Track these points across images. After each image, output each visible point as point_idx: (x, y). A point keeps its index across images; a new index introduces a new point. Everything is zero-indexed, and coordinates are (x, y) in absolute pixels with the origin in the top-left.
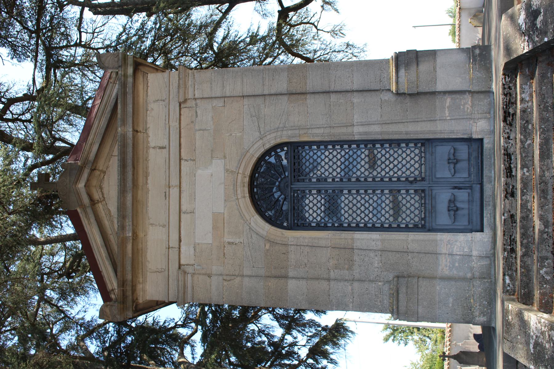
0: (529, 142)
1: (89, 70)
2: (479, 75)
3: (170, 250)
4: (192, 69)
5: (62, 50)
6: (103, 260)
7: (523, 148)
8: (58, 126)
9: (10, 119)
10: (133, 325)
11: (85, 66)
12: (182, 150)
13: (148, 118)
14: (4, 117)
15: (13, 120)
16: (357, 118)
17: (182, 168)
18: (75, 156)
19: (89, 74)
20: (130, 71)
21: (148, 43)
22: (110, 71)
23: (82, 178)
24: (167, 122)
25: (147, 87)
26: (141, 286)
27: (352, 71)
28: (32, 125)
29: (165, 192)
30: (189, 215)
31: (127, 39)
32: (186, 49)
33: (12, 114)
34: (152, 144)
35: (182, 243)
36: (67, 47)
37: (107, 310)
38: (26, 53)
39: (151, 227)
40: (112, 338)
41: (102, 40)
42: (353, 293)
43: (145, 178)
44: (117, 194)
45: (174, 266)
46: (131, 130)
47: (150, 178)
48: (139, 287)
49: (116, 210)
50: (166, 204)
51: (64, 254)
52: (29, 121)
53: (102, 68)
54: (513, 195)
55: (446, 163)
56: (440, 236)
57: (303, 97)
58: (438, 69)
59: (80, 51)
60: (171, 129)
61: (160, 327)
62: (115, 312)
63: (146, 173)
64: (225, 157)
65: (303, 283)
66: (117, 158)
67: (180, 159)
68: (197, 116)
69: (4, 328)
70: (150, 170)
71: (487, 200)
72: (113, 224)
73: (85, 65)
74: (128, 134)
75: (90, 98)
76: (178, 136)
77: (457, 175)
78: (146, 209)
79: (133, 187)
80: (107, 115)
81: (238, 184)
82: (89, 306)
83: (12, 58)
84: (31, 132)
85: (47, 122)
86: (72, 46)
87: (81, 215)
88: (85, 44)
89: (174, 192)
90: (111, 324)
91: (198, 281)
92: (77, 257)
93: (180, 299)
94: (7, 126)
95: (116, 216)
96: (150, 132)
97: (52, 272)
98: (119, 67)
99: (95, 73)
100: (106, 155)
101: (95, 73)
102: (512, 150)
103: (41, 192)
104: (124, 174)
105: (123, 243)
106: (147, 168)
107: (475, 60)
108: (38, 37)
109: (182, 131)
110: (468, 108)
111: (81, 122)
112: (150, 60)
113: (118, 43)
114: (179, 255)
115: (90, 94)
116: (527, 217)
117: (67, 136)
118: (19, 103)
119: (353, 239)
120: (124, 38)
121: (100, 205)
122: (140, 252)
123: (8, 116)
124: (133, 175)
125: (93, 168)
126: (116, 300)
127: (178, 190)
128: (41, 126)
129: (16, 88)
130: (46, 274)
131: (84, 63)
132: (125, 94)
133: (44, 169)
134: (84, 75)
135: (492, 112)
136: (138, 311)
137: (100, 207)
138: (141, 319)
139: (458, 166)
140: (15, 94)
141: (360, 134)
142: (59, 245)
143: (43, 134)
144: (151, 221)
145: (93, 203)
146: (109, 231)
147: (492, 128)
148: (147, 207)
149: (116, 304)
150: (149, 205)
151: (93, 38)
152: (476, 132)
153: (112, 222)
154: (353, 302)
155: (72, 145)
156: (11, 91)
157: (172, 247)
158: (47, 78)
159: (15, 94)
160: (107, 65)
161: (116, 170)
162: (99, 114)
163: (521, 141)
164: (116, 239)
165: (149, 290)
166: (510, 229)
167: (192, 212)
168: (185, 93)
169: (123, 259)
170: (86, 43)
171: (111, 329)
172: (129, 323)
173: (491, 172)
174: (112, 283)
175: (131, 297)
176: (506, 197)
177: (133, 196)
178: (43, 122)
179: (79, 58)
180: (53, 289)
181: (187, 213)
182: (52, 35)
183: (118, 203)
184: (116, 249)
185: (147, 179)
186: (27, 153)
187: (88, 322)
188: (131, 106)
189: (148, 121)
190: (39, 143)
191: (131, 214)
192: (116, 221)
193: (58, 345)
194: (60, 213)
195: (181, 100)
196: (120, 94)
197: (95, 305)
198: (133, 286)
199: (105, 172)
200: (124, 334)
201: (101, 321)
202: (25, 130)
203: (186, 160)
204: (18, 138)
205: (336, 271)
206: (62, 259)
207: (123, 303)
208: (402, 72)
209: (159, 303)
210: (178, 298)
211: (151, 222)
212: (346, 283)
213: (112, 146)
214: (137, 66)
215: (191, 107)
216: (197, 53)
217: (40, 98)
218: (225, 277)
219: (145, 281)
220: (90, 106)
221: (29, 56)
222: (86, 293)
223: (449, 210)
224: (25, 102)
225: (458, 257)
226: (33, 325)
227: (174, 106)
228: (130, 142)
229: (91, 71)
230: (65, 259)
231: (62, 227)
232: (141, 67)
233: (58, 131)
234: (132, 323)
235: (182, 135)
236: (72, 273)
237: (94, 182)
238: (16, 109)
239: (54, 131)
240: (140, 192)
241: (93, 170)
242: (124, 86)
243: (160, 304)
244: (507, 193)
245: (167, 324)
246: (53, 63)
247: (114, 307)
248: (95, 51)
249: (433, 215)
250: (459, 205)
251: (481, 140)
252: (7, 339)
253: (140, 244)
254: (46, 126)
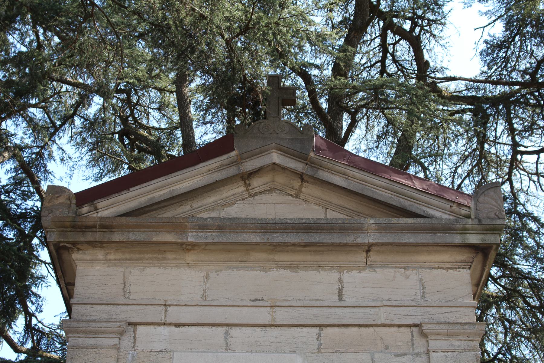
1: (473, 167)
3: (162, 308)
4: (482, 345)
5: (506, 121)
6: (148, 192)
8: (376, 117)
9: (386, 41)
10: (35, 241)
11: (480, 160)
12: (336, 329)
13: (392, 270)
14: (389, 32)
15: (384, 46)
17: (305, 329)
18: (324, 147)
19: (466, 167)
20: (474, 239)
21: (524, 266)
22: (472, 204)
23: (287, 159)
24: (385, 303)
25: (447, 269)
26: (101, 257)
28: (377, 75)
29: (262, 300)
30: (222, 341)
31: (530, 231)
32: (518, 334)
33: (394, 44)
34: (347, 277)
35: (173, 328)
36: (512, 131)
37: (62, 200)
38: (496, 64)
40: (13, 206)
41: (525, 189)
43: (288, 264)
44: (261, 217)
46: (371, 241)
47: (287, 273)
48: (100, 254)
49: (233, 215)
50: (242, 300)
51: (163, 126)
52: (383, 71)
53: (476, 191)
59: (505, 151)
60: (374, 310)
61: (28, 288)
62: (58, 212)
63: (297, 267)
66: (323, 217)
67: (320, 326)
68: (397, 355)
69: (41, 31)
70: (302, 274)
72: (210, 210)
73: (481, 160)
74: (363, 235)
75: (425, 169)
76: (361, 322)
78: (233, 267)
79: (271, 244)
80: (396, 200)
82: (71, 169)
83: (486, 42)
84: (365, 74)
85: (382, 100)
86: (513, 139)
87: (225, 157)
88: (517, 160)
89: (263, 315)
90: (39, 204)
91: (105, 357)
92: (156, 148)
93: (75, 324)
94: (374, 36)
95: (222, 215)
96: (367, 274)
97: (132, 106)
98: (480, 221)
99: (468, 176)
100: (327, 198)
101: (468, 176)
103: (263, 93)
104: (294, 228)
105: (176, 226)
106: (306, 268)
108: (523, 85)
109: (371, 329)
111: (381, 156)
112: (494, 271)
113: (521, 216)
114: (152, 324)
115: (431, 168)
117: (359, 131)
118: (413, 54)
120: (533, 226)
121: (243, 188)
122: (159, 256)
123: (391, 38)
124: (293, 245)
125: (304, 177)
127: (267, 323)
128: (376, 91)
129: (437, 49)
130: (129, 96)
131: (485, 158)
132: (433, 230)
133: (303, 98)
134: (464, 159)
136: (57, 251)
137: (239, 189)
138: (44, 255)
140: (428, 48)
142: (176, 118)
143: (361, 94)
144: (212, 275)
145: (246, 177)
146: (197, 204)
148: (238, 269)
149: (71, 214)
150: (242, 272)
151: (528, 173)
155: (346, 139)
156: (433, 41)
157: (166, 311)
158: (455, 98)
159: (428, 48)
160: (481, 199)
161: (302, 216)
162: (397, 187)
164: (183, 216)
165: (95, 272)
167: (227, 347)
168: (438, 334)
169: (149, 227)
170: (520, 162)
171: (30, 203)
172: (39, 234)
174: (108, 208)
175: (82, 239)
177: (257, 244)
178: (383, 93)
179: (493, 150)
180: (104, 109)
181: (226, 339)
182: (530, 105)
183: (244, 219)
184: (164, 216)
185: (285, 268)
186: (330, 68)
187: (45, 166)
188: (412, 240)
189: (386, 270)
190: (346, 86)
191: (225, 240)
192: (214, 214)
193: (9, 116)
194: (230, 121)
195: (425, 328)
196: (433, 221)
197: (71, 177)
198: (101, 242)
199: (297, 196)
200: (19, 225)
201: (44, 186)
202: (369, 64)
203: (319, 336)
204: (354, 54)
206: (154, 123)
209: (70, 287)
210: (77, 321)
211: (211, 275)
213: (341, 209)
214: (483, 250)
215: (413, 344)
216: (511, 354)
217: (421, 88)
219: (108, 263)
220: (412, 170)
221: (490, 68)
222: (95, 161)
224: (414, 63)
226: (47, 76)
227: (414, 316)
228: (350, 239)
229: (471, 171)
230: (153, 128)
231: (205, 124)
232: (480, 257)
233: (368, 118)
234: (38, 238)
235: (363, 329)
236: (128, 138)
237: (280, 179)
238: (403, 51)
239: (367, 112)
240: (263, 256)
241: (301, 177)
242: (447, 228)
243: (68, 290)
245: (33, 299)
246: (481, 108)
247: (66, 210)
248: (507, 177)
252: (23, 36)
253: (174, 256)
254: (376, 98)
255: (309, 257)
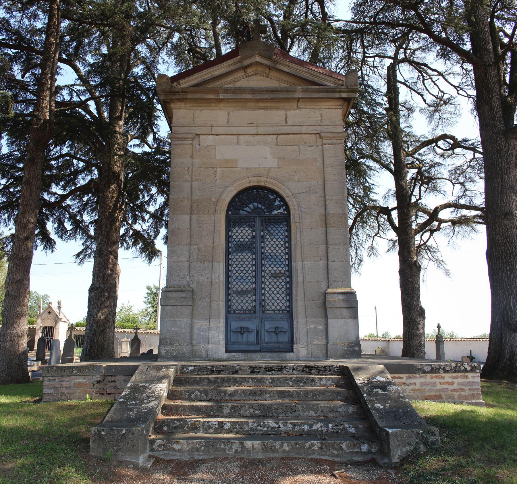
0: (291, 383)
2: (340, 350)
7: (287, 379)
12: (284, 135)
16: (307, 264)
20: (344, 95)
23: (263, 60)
25: (332, 109)
27: (342, 261)
39: (227, 112)
42: (181, 262)
43: (263, 107)
45: (198, 130)
47: (263, 111)
48: (182, 104)
54: (252, 372)
55: (276, 326)
56: (222, 321)
57: (324, 225)
58: (344, 320)
64: (279, 168)
65: (187, 226)
67: (277, 134)
68: (310, 146)
70: (270, 112)
71: (249, 355)
77: (266, 333)
81: (259, 178)
87: (235, 59)
89: (253, 130)
96: (297, 111)
102: (285, 372)
107: (350, 346)
109: (299, 135)
110: (315, 341)
116: (237, 382)
119: (220, 261)
121: (243, 73)
124: (266, 99)
126: (172, 87)
132: (327, 91)
135: (312, 359)
137: (241, 74)
139: (273, 334)
141: (296, 267)
145: (245, 68)
147: (301, 359)
150: (244, 111)
152: (298, 347)
153: (230, 83)
154: (174, 262)
163: (291, 378)
166: (228, 370)
173: (269, 358)
176: (251, 367)
185: (262, 109)
188: (317, 96)
192: (231, 86)
199: (267, 77)
205: (196, 249)
207: (170, 92)
208: (341, 297)
212: (188, 257)
218: (190, 168)
223: (241, 328)
225: (207, 334)
228: (290, 96)
235: (295, 135)
237: (260, 69)
240: (253, 104)
242: (333, 90)
244: (254, 368)
249: (237, 319)
250: (245, 335)
251: (292, 351)
255: (272, 104)
